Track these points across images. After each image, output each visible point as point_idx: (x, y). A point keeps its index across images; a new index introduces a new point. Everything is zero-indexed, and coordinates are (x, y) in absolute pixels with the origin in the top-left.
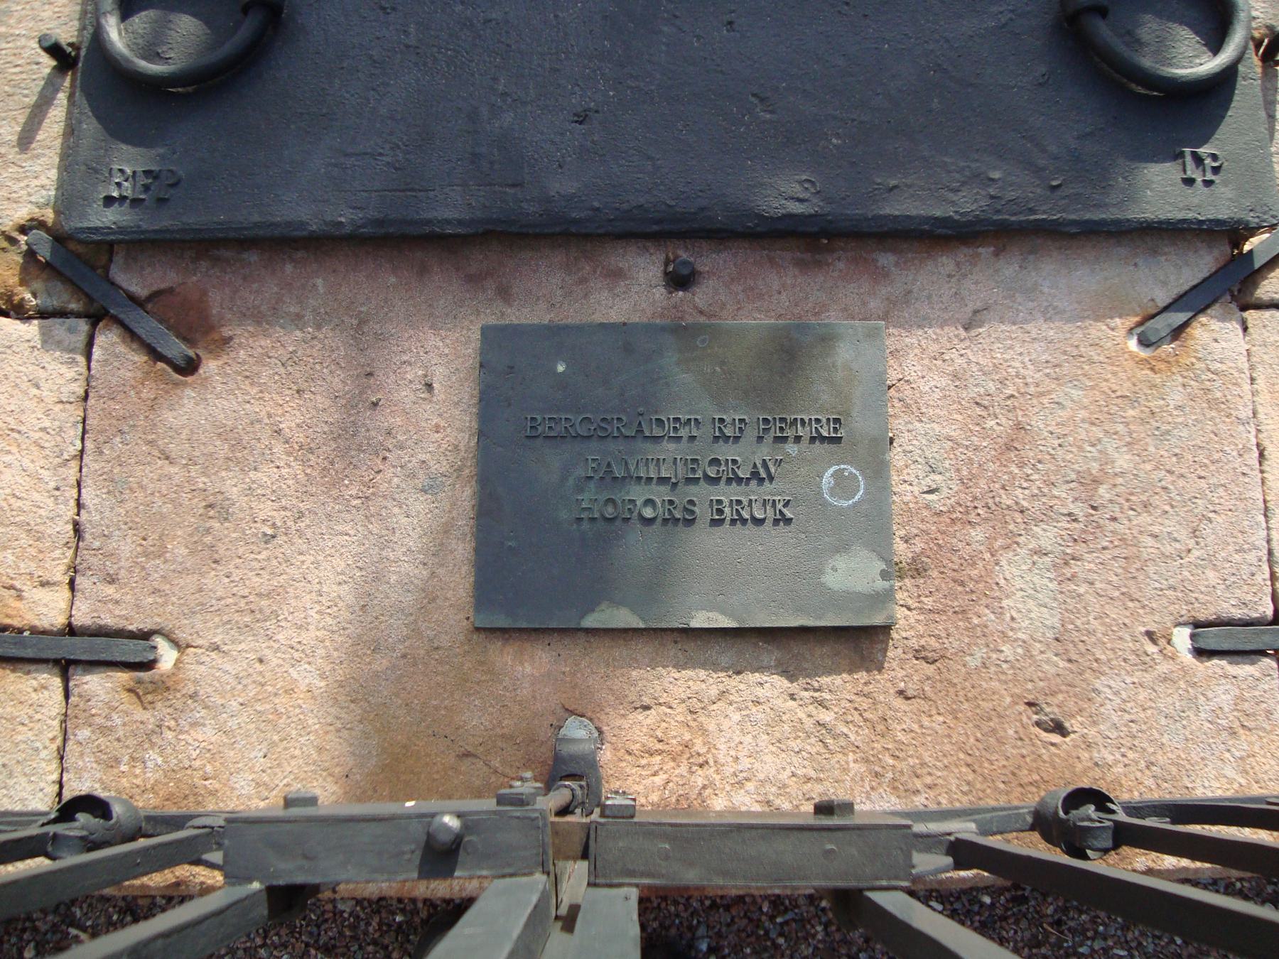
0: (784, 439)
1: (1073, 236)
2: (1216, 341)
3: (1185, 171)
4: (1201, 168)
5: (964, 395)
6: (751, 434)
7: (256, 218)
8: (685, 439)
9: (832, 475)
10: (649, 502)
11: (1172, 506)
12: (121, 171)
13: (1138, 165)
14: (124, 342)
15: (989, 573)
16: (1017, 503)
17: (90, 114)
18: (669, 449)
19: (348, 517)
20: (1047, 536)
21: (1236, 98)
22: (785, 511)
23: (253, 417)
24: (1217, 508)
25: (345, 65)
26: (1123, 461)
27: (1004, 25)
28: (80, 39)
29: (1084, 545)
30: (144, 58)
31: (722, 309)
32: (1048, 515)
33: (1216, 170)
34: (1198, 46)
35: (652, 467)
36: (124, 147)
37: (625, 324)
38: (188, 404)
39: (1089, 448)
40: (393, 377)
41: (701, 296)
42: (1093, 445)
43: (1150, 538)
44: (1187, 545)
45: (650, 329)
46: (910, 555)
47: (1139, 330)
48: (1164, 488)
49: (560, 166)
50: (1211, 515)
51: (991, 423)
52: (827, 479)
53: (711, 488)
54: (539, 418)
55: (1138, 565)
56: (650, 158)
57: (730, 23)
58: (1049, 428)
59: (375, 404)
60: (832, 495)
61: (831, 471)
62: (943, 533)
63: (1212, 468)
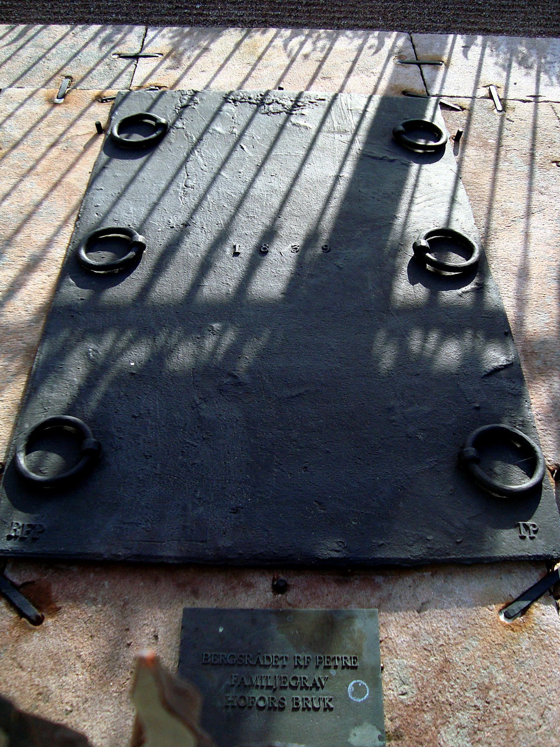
0: (329, 667)
1: (469, 566)
2: (544, 615)
3: (521, 533)
4: (528, 531)
5: (418, 645)
6: (313, 664)
7: (79, 550)
8: (280, 666)
9: (353, 685)
10: (262, 698)
11: (529, 702)
12: (17, 524)
13: (498, 530)
14: (7, 606)
15: (435, 738)
16: (447, 700)
17: (6, 496)
18: (271, 672)
19: (111, 702)
20: (464, 717)
21: (542, 498)
22: (330, 704)
23: (67, 648)
24: (553, 702)
25: (126, 481)
26: (501, 678)
27: (433, 468)
28: (5, 461)
29: (484, 723)
30: (34, 472)
31: (299, 603)
32: (464, 707)
33: (535, 532)
34: (523, 475)
35: (264, 680)
36: (20, 512)
37: (252, 609)
38: (35, 640)
39: (482, 671)
40: (139, 631)
41: (290, 596)
42: (485, 669)
43: (518, 719)
44: (538, 723)
45: (265, 612)
46: (394, 728)
47: (505, 610)
48: (524, 692)
49: (224, 533)
50: (550, 706)
51: (432, 659)
52: (350, 687)
53: (293, 691)
54: (209, 654)
55: (514, 734)
56: (267, 531)
57: (305, 468)
58: (462, 661)
59: (129, 645)
60: (353, 695)
61: (352, 683)
62: (410, 716)
63: (548, 680)
